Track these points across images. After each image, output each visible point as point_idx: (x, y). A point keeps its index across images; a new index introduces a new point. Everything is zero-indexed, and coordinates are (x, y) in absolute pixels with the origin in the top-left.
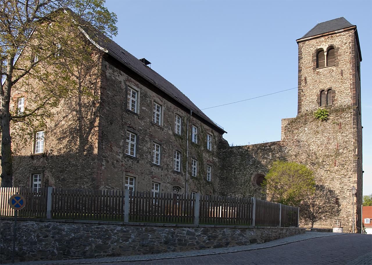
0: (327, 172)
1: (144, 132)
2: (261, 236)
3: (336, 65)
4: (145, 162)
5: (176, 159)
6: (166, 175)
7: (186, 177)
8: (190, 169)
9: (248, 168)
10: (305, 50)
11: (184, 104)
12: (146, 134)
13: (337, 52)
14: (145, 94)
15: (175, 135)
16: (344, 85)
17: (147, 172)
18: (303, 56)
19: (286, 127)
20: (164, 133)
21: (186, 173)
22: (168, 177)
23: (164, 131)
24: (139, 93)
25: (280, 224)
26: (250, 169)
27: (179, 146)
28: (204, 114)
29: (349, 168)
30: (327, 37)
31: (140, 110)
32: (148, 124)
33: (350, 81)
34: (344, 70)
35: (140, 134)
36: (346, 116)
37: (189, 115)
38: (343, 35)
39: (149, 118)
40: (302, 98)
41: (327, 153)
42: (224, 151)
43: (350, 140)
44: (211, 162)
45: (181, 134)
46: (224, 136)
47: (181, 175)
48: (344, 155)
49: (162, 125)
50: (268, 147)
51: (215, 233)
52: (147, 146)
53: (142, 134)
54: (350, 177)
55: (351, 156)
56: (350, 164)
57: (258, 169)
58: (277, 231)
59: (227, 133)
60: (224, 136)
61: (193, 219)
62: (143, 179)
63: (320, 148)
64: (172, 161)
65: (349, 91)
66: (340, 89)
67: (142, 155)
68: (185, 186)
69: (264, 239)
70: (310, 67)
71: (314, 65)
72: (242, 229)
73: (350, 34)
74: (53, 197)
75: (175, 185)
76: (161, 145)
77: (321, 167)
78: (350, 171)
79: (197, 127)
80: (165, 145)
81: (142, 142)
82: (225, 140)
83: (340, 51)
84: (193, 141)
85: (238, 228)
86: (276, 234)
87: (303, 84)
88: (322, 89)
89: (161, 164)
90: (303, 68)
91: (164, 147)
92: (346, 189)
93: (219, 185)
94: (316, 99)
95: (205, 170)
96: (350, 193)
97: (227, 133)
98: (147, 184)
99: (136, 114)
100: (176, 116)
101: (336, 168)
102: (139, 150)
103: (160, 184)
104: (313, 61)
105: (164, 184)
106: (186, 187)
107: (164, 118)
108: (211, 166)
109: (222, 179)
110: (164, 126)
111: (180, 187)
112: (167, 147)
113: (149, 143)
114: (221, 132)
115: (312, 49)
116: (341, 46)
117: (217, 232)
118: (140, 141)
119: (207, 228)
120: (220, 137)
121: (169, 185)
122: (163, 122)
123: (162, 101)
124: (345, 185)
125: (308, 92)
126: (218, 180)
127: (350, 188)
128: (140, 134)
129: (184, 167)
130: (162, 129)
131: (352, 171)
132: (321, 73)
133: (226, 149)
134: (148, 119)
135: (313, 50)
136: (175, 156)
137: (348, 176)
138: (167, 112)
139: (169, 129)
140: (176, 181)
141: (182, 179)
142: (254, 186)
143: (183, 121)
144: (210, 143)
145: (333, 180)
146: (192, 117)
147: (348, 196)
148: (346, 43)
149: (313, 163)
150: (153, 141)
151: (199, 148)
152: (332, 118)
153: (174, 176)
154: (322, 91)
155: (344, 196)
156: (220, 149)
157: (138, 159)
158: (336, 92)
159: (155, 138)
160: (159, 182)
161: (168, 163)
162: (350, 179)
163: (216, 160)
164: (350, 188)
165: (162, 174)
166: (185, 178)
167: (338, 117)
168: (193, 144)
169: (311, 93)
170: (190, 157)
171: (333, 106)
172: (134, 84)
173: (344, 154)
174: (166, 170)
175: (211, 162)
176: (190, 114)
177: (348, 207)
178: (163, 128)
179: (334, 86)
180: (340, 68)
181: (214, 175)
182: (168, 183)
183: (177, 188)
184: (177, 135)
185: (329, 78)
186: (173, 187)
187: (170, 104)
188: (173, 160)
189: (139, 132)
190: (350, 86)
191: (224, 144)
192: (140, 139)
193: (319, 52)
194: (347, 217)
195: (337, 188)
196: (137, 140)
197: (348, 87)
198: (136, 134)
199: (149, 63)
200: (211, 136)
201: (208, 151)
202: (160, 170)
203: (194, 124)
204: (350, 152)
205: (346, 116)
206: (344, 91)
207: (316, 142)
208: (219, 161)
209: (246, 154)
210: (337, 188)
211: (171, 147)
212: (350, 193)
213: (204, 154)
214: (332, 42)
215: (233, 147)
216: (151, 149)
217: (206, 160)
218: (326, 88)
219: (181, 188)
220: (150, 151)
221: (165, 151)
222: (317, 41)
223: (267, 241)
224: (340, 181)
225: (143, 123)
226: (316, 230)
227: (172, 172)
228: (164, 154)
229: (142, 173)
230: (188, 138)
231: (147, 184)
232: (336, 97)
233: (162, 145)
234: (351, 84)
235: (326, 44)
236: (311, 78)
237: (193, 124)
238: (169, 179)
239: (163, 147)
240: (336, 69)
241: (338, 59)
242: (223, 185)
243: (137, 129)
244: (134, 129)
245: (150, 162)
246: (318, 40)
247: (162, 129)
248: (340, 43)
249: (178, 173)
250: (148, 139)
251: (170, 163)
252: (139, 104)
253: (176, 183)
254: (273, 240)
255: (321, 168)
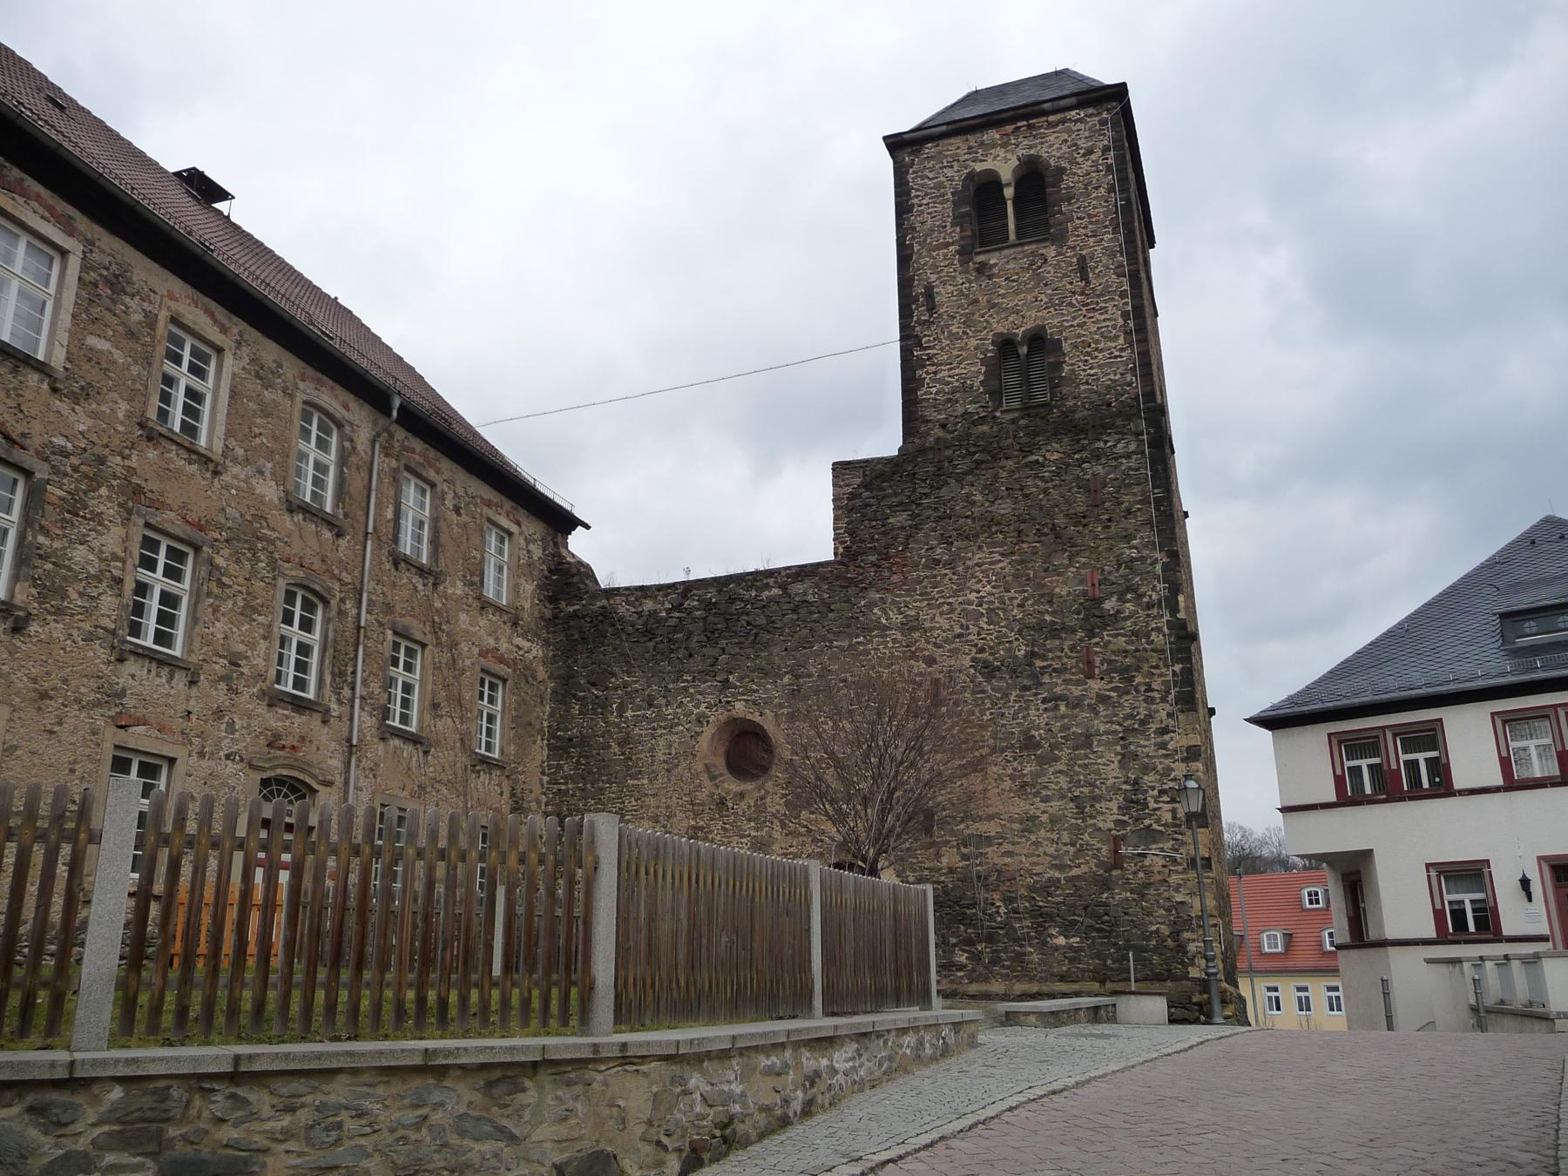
0: (1057, 707)
1: (84, 468)
2: (650, 1123)
3: (1060, 239)
4: (75, 633)
5: (295, 632)
6: (219, 713)
7: (351, 731)
8: (375, 687)
9: (685, 689)
10: (923, 178)
11: (323, 325)
12: (95, 482)
13: (1056, 184)
14: (117, 276)
15: (293, 506)
16: (1097, 315)
17: (83, 690)
18: (915, 201)
19: (852, 497)
20: (227, 487)
21: (352, 707)
22: (231, 724)
23: (226, 478)
24: (74, 263)
25: (818, 1001)
26: (691, 695)
27: (317, 565)
28: (447, 405)
29: (1155, 686)
30: (1010, 128)
31: (72, 350)
32: (121, 429)
33: (1119, 302)
34: (1092, 258)
35: (55, 470)
36: (1120, 448)
37: (383, 422)
38: (1076, 121)
39: (130, 400)
40: (919, 372)
41: (1048, 618)
42: (571, 609)
43: (1145, 552)
44: (501, 660)
45: (336, 506)
46: (578, 544)
47: (317, 716)
48: (1129, 623)
49: (218, 446)
50: (776, 591)
51: (235, 1126)
52: (96, 544)
53: (66, 475)
54: (1164, 731)
55: (1159, 630)
56: (1157, 667)
57: (733, 695)
58: (787, 1066)
59: (587, 527)
60: (578, 544)
61: (58, 1000)
62: (51, 732)
63: (1012, 594)
64: (265, 638)
65: (1121, 341)
66: (1079, 336)
67: (50, 590)
68: (339, 780)
69: (679, 1150)
70: (947, 245)
71: (962, 238)
72: (497, 1074)
73: (1105, 115)
74: (145, 865)
75: (279, 771)
76: (197, 549)
77: (1027, 682)
78: (1164, 700)
79: (433, 485)
80: (226, 552)
81: (64, 520)
82: (580, 563)
83: (1067, 181)
84: (406, 546)
85: (461, 1067)
86: (776, 1082)
87: (920, 313)
88: (1001, 334)
89: (191, 652)
90: (916, 247)
91: (220, 561)
92: (1153, 788)
93: (546, 779)
94: (981, 378)
95: (467, 696)
96: (1174, 811)
97: (587, 527)
98: (75, 762)
99: (42, 368)
100: (312, 414)
101: (1095, 685)
102: (38, 562)
103: (172, 761)
104: (958, 220)
105: (204, 763)
106: (346, 783)
107: (229, 414)
108: (505, 681)
109: (560, 748)
110: (224, 455)
111: (308, 780)
112: (238, 561)
113: (117, 531)
114: (562, 521)
115: (949, 172)
116: (1071, 163)
117: (253, 1116)
118: (51, 516)
119: (161, 1084)
120: (556, 544)
121: (231, 767)
122: (221, 430)
123: (224, 330)
124: (1146, 769)
125: (942, 349)
126: (539, 751)
127: (1171, 784)
128: (55, 470)
129: (341, 674)
130: (211, 466)
131: (1171, 697)
132: (996, 270)
133: (581, 599)
134: (124, 406)
135: (954, 176)
136: (482, 693)
137: (1154, 726)
138: (254, 386)
139: (261, 472)
140: (284, 747)
141: (324, 738)
142: (713, 778)
143: (347, 444)
144: (500, 569)
145: (1090, 746)
146: (400, 434)
147: (1165, 825)
148: (1090, 152)
149: (986, 664)
150: (141, 522)
151: (435, 585)
152: (1056, 456)
153: (278, 719)
154: (1006, 345)
155: (1147, 822)
156: (553, 600)
157: (21, 614)
158: (1066, 347)
159: (158, 505)
160: (168, 751)
161: (242, 648)
162: (1167, 737)
163: (534, 652)
164: (1171, 784)
165: (194, 706)
166: (345, 734)
167: (1084, 454)
168: (398, 560)
169: (955, 353)
170: (381, 624)
171: (1057, 407)
172: (41, 210)
173: (1125, 619)
174: (223, 685)
175: (501, 660)
176: (389, 415)
177: (1174, 879)
178: (219, 459)
179: (1051, 322)
180: (1074, 248)
181: (520, 725)
182: (228, 757)
183: (293, 789)
184: (305, 510)
185: (1030, 291)
186: (265, 783)
187: (271, 352)
188: (270, 632)
189: (46, 459)
190: (1121, 321)
191: (567, 580)
192: (53, 499)
193: (984, 190)
194: (1176, 934)
195: (1109, 783)
196: (26, 507)
197: (1114, 326)
198: (28, 474)
199: (224, 195)
200: (510, 534)
201: (485, 605)
202: (180, 680)
203: (413, 465)
204: (1155, 611)
205: (1120, 448)
206: (1097, 342)
207: (992, 563)
208: (545, 656)
209: (672, 622)
210: (1109, 783)
211: (262, 565)
212: (1174, 811)
213: (463, 617)
214: (1031, 147)
215: (612, 592)
216: (124, 562)
217: (476, 650)
218: (1020, 331)
219: (314, 791)
220: (116, 573)
221: (224, 579)
222: (972, 144)
223: (706, 1156)
224: (1119, 748)
225: (83, 418)
226: (1032, 1019)
227: (263, 694)
228: (217, 597)
229: (44, 695)
230: (370, 530)
231: (75, 762)
232: (1066, 368)
233: (205, 548)
234: (1125, 315)
235: (1009, 156)
236: (950, 288)
237: (408, 468)
238: (237, 735)
239: (211, 563)
240: (1059, 254)
241: (1060, 212)
242: (565, 778)
243: (36, 441)
244: (14, 442)
245: (113, 633)
246: (973, 139)
247: (211, 466)
248: (1065, 149)
249: (300, 705)
250: (110, 510)
251: (252, 646)
252: (66, 319)
253: (281, 762)
254: (761, 1136)
255: (1026, 688)
